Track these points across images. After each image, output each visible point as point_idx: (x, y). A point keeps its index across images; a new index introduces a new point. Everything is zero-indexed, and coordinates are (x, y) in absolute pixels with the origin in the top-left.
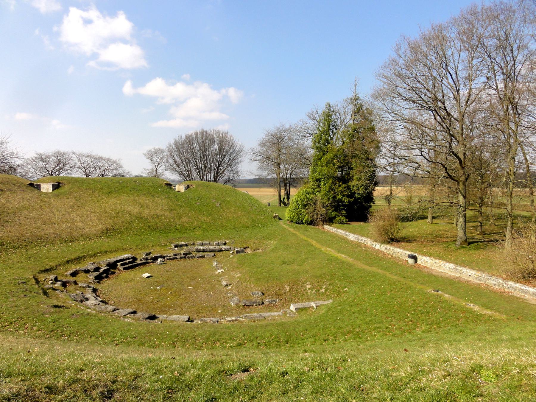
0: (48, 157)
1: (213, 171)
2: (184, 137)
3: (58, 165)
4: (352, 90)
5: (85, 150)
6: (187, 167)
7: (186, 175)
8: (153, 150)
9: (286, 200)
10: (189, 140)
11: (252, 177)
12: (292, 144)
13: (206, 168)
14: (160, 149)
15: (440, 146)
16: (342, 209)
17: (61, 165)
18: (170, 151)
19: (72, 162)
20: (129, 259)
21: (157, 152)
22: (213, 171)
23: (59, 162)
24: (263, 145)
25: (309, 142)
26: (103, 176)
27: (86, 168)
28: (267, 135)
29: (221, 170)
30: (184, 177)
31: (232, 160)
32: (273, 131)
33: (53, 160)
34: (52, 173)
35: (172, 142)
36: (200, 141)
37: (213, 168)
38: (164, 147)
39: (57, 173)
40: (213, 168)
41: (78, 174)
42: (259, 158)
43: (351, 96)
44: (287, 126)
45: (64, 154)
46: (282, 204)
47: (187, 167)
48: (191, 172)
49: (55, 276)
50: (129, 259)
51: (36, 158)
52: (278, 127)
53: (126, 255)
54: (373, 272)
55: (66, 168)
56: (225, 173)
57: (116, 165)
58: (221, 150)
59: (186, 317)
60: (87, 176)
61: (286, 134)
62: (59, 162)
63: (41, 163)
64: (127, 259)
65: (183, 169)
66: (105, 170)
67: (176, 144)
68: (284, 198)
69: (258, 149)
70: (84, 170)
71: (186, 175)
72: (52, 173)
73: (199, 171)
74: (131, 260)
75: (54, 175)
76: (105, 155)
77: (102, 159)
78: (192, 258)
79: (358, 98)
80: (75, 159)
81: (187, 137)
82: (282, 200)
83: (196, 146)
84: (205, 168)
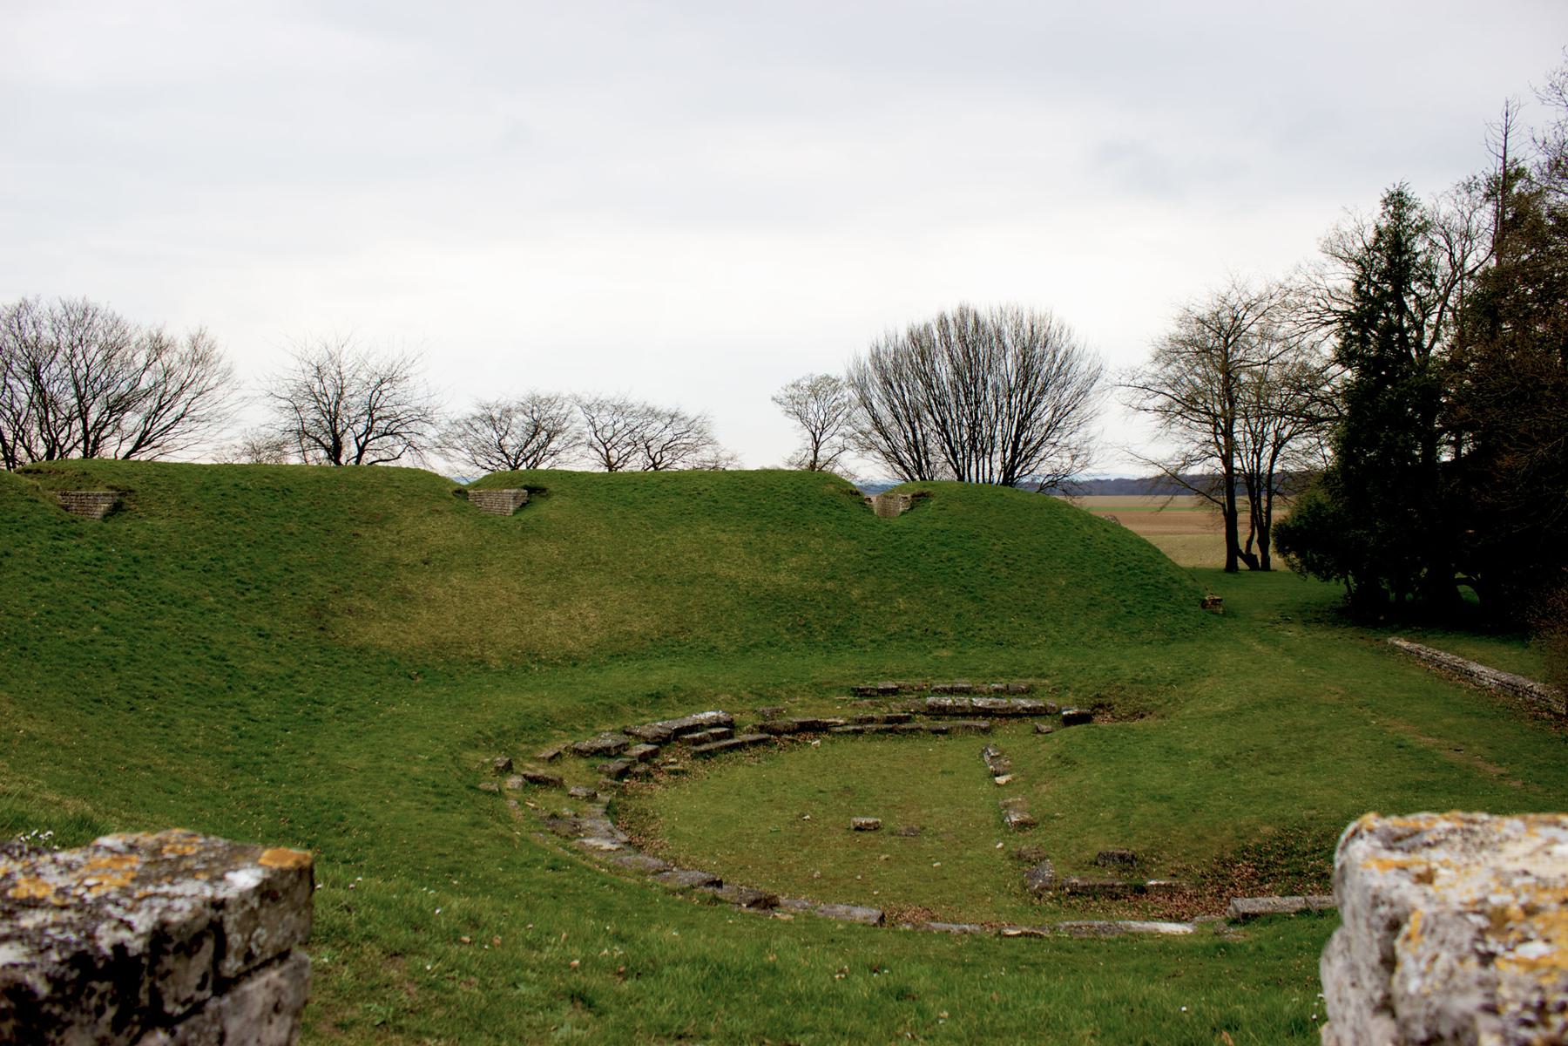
0: (507, 412)
1: (998, 448)
2: (903, 335)
3: (533, 437)
4: (1493, 147)
5: (610, 390)
6: (915, 436)
7: (910, 464)
8: (806, 383)
9: (1256, 550)
10: (920, 347)
11: (1151, 472)
12: (1276, 348)
13: (975, 441)
14: (827, 377)
15: (342, 388)
16: (1461, 581)
17: (543, 435)
18: (861, 386)
19: (572, 432)
20: (718, 725)
21: (821, 388)
22: (998, 448)
23: (536, 427)
24: (1167, 355)
25: (1328, 343)
26: (656, 469)
27: (609, 446)
28: (1182, 321)
29: (1026, 444)
30: (905, 469)
31: (1060, 413)
32: (1204, 307)
33: (520, 419)
34: (516, 461)
35: (865, 355)
36: (958, 349)
37: (999, 439)
38: (839, 369)
39: (531, 460)
40: (999, 439)
41: (584, 461)
42: (1161, 400)
43: (1494, 168)
44: (1256, 289)
45: (550, 401)
46: (1241, 564)
47: (915, 436)
48: (926, 453)
49: (507, 759)
50: (718, 725)
51: (474, 418)
52: (1224, 292)
53: (709, 714)
54: (1171, 636)
55: (553, 445)
56: (1041, 454)
57: (694, 432)
58: (1026, 371)
59: (874, 914)
60: (610, 470)
61: (1250, 317)
62: (537, 430)
63: (490, 431)
64: (712, 726)
65: (902, 443)
66: (664, 448)
67: (876, 357)
68: (1249, 543)
69: (1150, 370)
70: (603, 451)
71: (910, 464)
72: (516, 461)
73: (952, 449)
74: (724, 729)
75: (523, 467)
76: (664, 404)
77: (654, 414)
78: (912, 730)
79: (1520, 173)
80: (580, 418)
81: (915, 338)
82: (1243, 547)
83: (944, 370)
84: (973, 439)
